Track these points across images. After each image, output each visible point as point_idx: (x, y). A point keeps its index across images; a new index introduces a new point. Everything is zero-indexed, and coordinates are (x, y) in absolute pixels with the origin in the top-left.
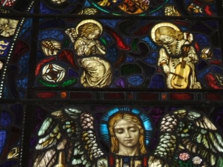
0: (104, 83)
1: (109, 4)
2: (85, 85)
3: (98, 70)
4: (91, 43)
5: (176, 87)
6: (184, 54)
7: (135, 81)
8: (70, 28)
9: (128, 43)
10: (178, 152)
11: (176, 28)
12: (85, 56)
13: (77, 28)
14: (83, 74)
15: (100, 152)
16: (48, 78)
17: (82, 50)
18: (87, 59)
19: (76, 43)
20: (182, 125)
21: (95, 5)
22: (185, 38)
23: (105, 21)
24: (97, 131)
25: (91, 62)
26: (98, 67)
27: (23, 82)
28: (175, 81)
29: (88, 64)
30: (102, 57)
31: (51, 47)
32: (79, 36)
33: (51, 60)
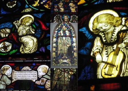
0: (33, 51)
1: (39, 5)
2: (22, 52)
3: (62, 10)
4: (27, 28)
5: (106, 77)
6: (74, 7)
7: (67, 11)
8: (16, 20)
9: (66, 6)
10: (73, 21)
11: (116, 14)
12: (23, 36)
13: (20, 20)
14: (21, 46)
16: (2, 50)
17: (22, 32)
18: (24, 37)
19: (19, 29)
21: (30, 6)
22: (123, 23)
23: (35, 15)
24: (62, 18)
25: (26, 39)
26: (30, 41)
28: (106, 71)
29: (24, 40)
30: (33, 35)
32: (21, 24)
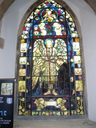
7: (51, 34)
10: (58, 47)
15: (45, 47)
20: (59, 42)
24: (44, 43)
27: (31, 35)
31: (36, 28)
33: (36, 31)
